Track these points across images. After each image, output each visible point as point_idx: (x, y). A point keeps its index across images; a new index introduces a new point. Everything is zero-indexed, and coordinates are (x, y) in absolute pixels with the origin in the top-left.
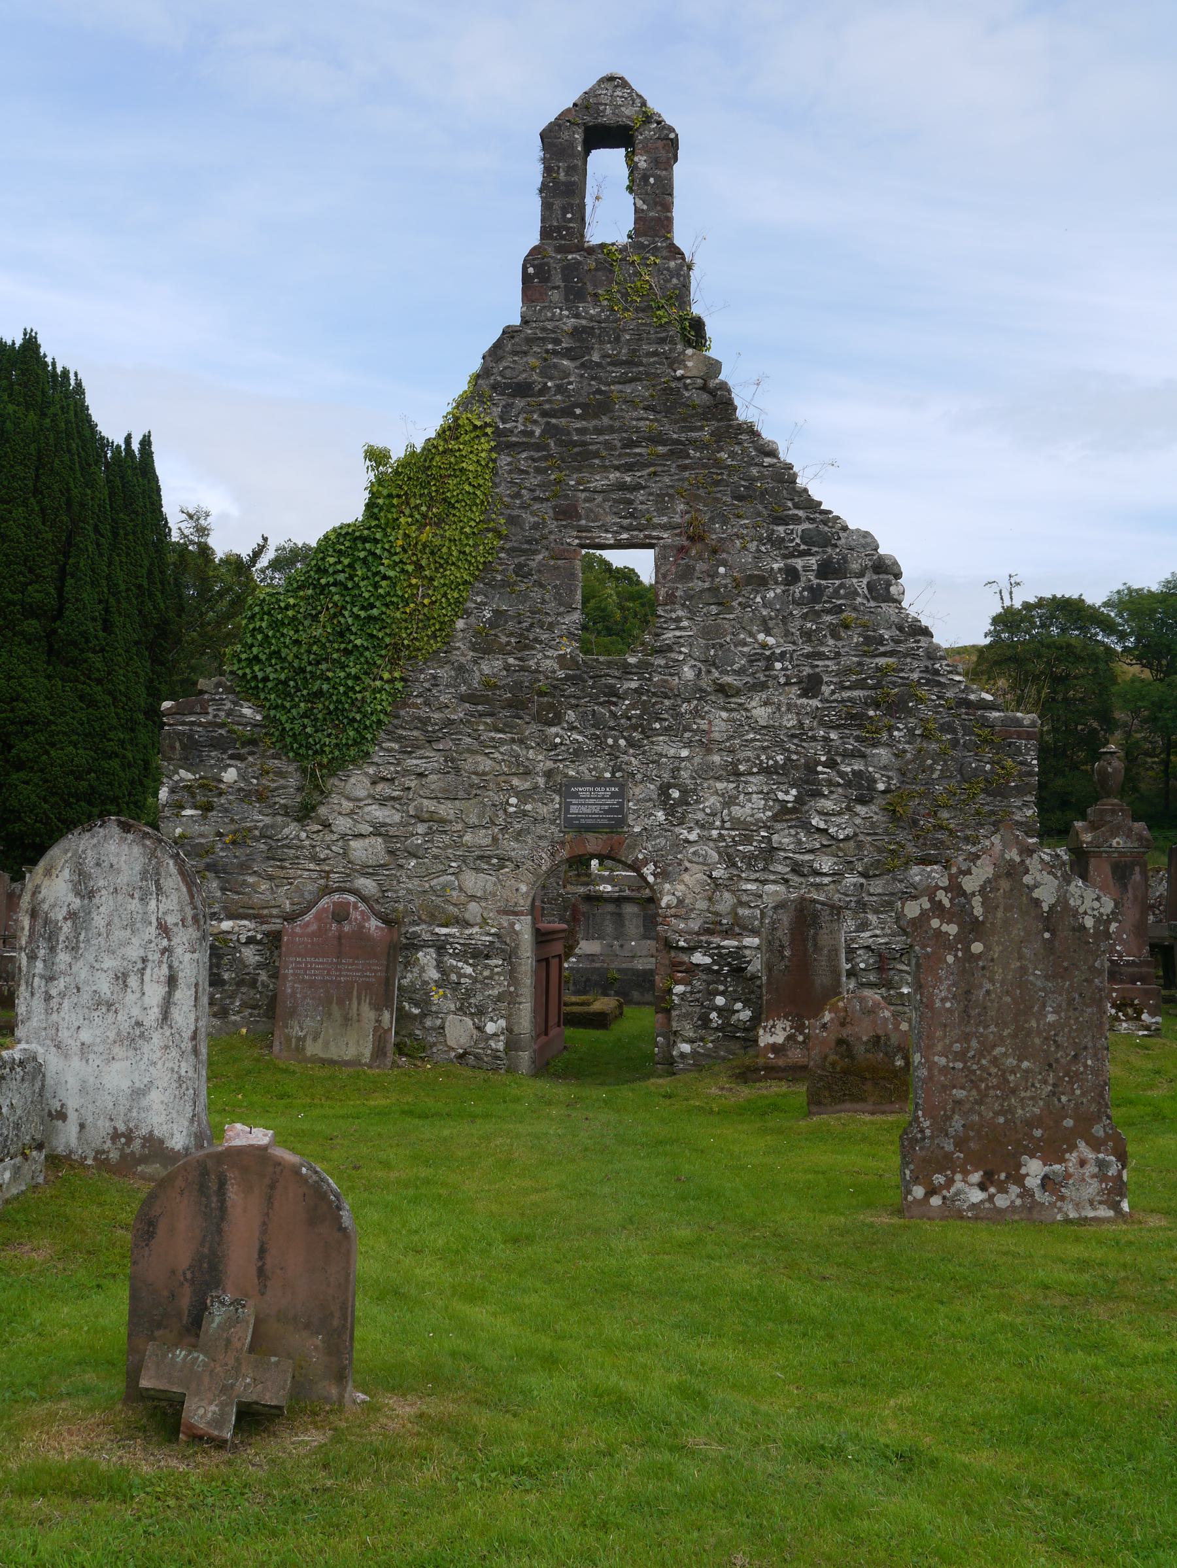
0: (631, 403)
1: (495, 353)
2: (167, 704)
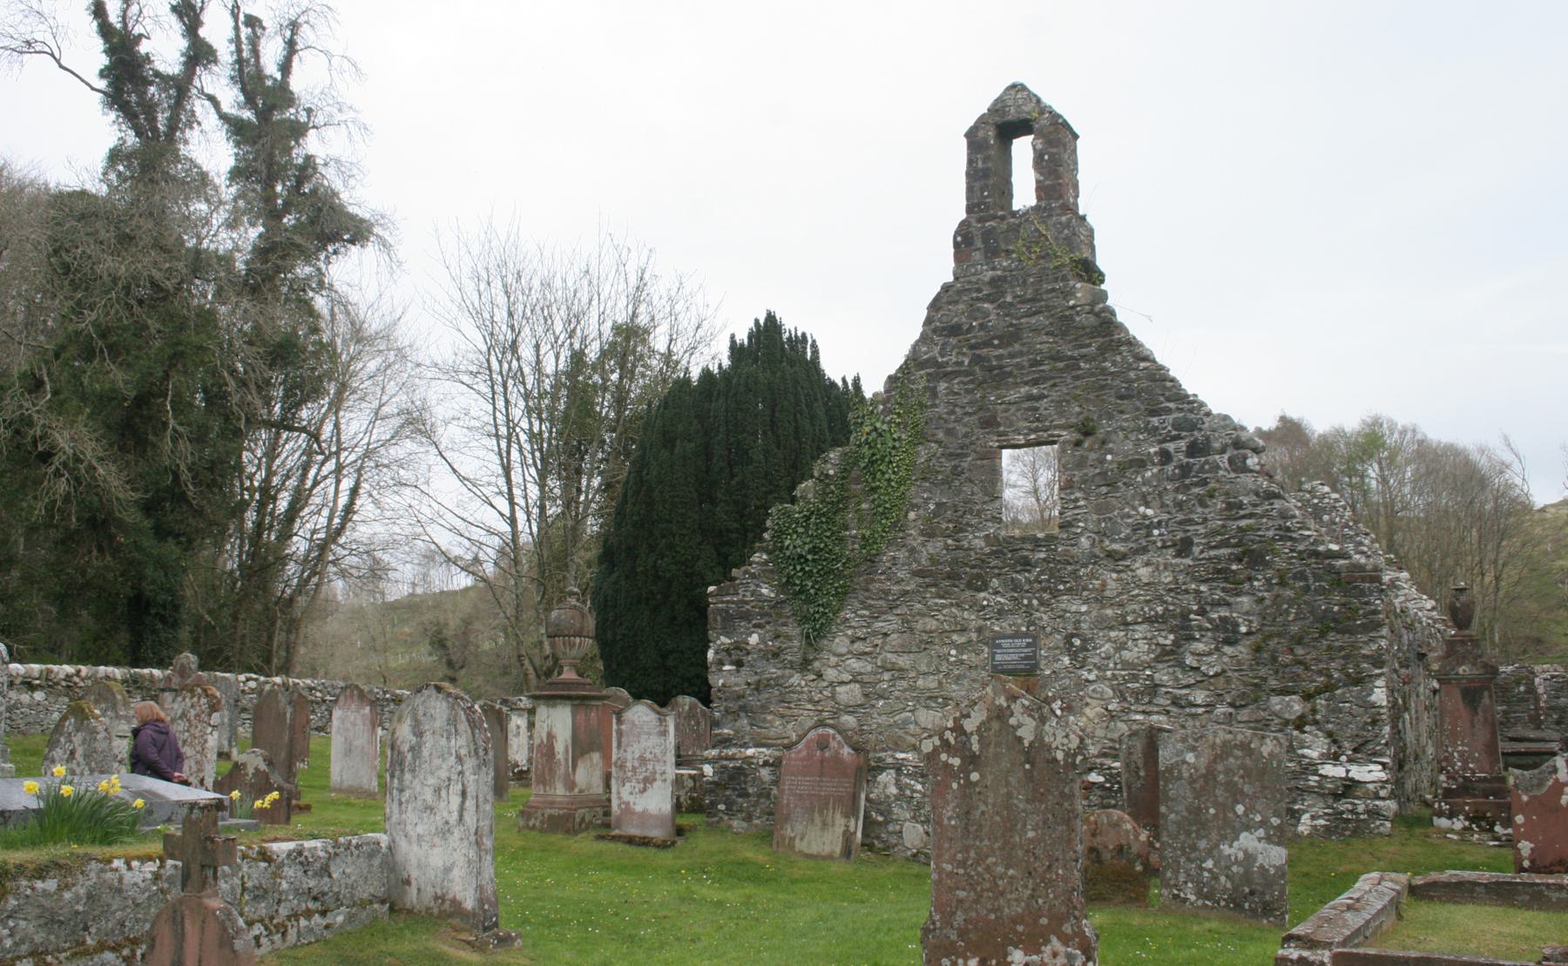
0: (1036, 331)
1: (935, 305)
2: (711, 589)
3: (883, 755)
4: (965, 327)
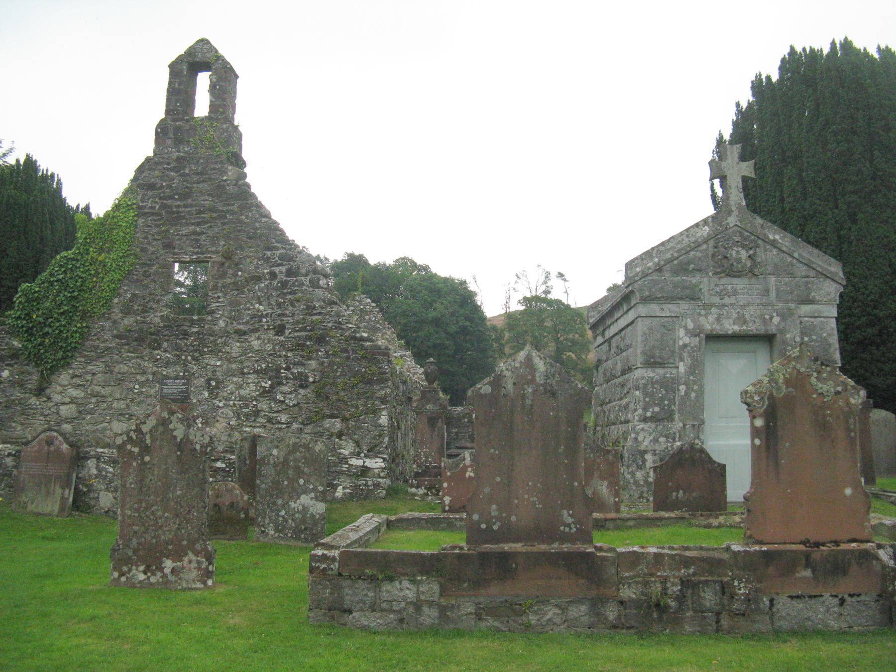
0: (201, 193)
1: (140, 170)
3: (88, 449)
4: (158, 186)
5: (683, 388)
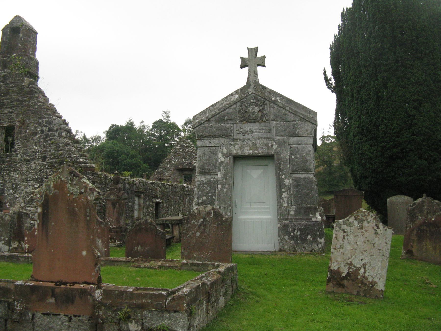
5: (220, 186)
